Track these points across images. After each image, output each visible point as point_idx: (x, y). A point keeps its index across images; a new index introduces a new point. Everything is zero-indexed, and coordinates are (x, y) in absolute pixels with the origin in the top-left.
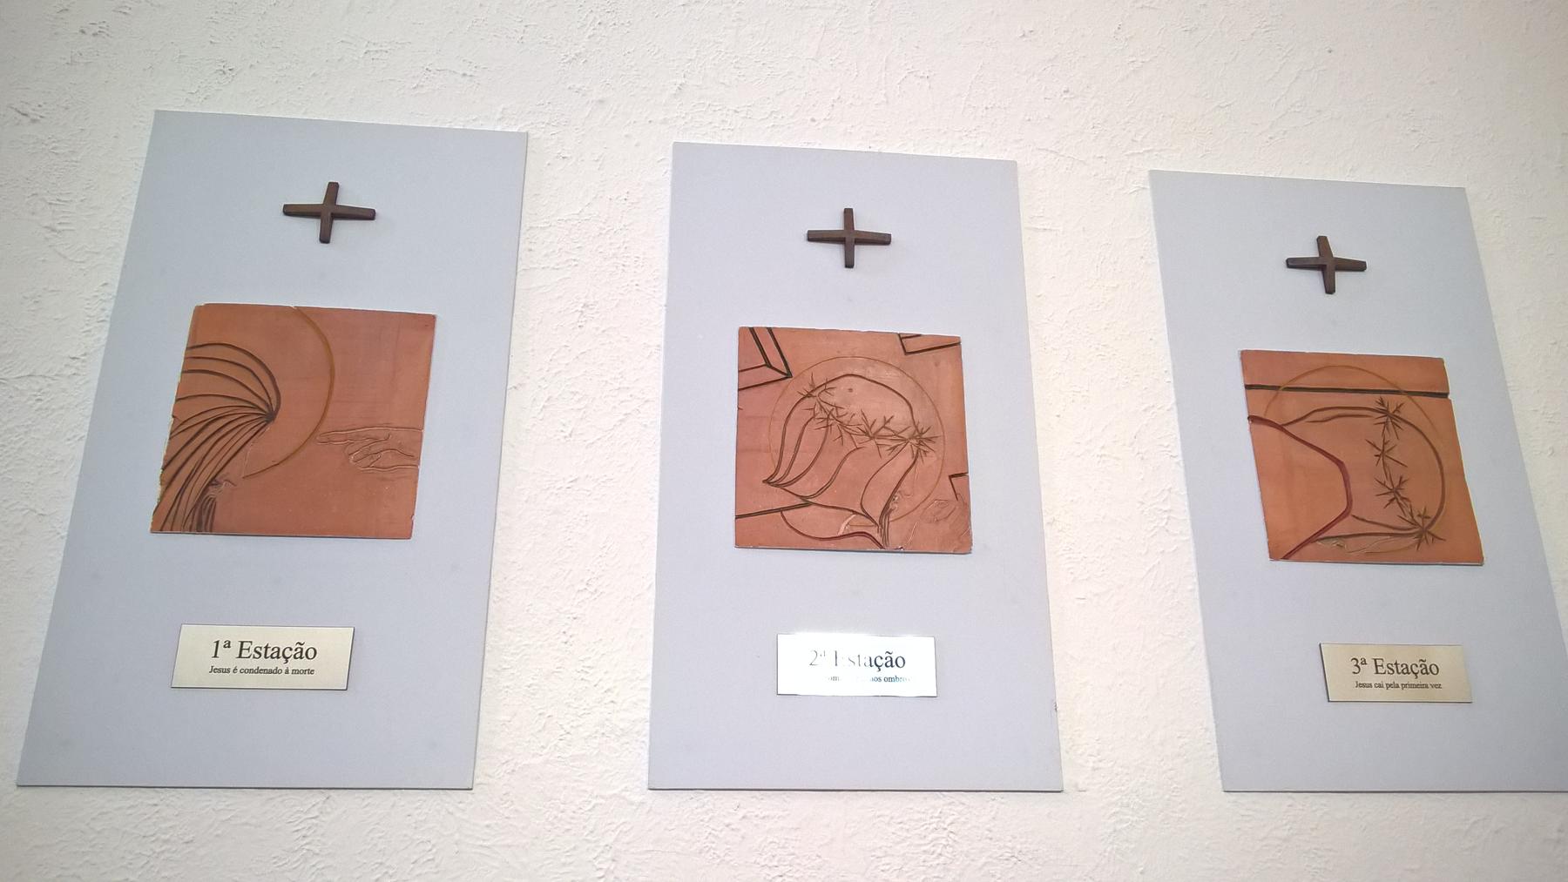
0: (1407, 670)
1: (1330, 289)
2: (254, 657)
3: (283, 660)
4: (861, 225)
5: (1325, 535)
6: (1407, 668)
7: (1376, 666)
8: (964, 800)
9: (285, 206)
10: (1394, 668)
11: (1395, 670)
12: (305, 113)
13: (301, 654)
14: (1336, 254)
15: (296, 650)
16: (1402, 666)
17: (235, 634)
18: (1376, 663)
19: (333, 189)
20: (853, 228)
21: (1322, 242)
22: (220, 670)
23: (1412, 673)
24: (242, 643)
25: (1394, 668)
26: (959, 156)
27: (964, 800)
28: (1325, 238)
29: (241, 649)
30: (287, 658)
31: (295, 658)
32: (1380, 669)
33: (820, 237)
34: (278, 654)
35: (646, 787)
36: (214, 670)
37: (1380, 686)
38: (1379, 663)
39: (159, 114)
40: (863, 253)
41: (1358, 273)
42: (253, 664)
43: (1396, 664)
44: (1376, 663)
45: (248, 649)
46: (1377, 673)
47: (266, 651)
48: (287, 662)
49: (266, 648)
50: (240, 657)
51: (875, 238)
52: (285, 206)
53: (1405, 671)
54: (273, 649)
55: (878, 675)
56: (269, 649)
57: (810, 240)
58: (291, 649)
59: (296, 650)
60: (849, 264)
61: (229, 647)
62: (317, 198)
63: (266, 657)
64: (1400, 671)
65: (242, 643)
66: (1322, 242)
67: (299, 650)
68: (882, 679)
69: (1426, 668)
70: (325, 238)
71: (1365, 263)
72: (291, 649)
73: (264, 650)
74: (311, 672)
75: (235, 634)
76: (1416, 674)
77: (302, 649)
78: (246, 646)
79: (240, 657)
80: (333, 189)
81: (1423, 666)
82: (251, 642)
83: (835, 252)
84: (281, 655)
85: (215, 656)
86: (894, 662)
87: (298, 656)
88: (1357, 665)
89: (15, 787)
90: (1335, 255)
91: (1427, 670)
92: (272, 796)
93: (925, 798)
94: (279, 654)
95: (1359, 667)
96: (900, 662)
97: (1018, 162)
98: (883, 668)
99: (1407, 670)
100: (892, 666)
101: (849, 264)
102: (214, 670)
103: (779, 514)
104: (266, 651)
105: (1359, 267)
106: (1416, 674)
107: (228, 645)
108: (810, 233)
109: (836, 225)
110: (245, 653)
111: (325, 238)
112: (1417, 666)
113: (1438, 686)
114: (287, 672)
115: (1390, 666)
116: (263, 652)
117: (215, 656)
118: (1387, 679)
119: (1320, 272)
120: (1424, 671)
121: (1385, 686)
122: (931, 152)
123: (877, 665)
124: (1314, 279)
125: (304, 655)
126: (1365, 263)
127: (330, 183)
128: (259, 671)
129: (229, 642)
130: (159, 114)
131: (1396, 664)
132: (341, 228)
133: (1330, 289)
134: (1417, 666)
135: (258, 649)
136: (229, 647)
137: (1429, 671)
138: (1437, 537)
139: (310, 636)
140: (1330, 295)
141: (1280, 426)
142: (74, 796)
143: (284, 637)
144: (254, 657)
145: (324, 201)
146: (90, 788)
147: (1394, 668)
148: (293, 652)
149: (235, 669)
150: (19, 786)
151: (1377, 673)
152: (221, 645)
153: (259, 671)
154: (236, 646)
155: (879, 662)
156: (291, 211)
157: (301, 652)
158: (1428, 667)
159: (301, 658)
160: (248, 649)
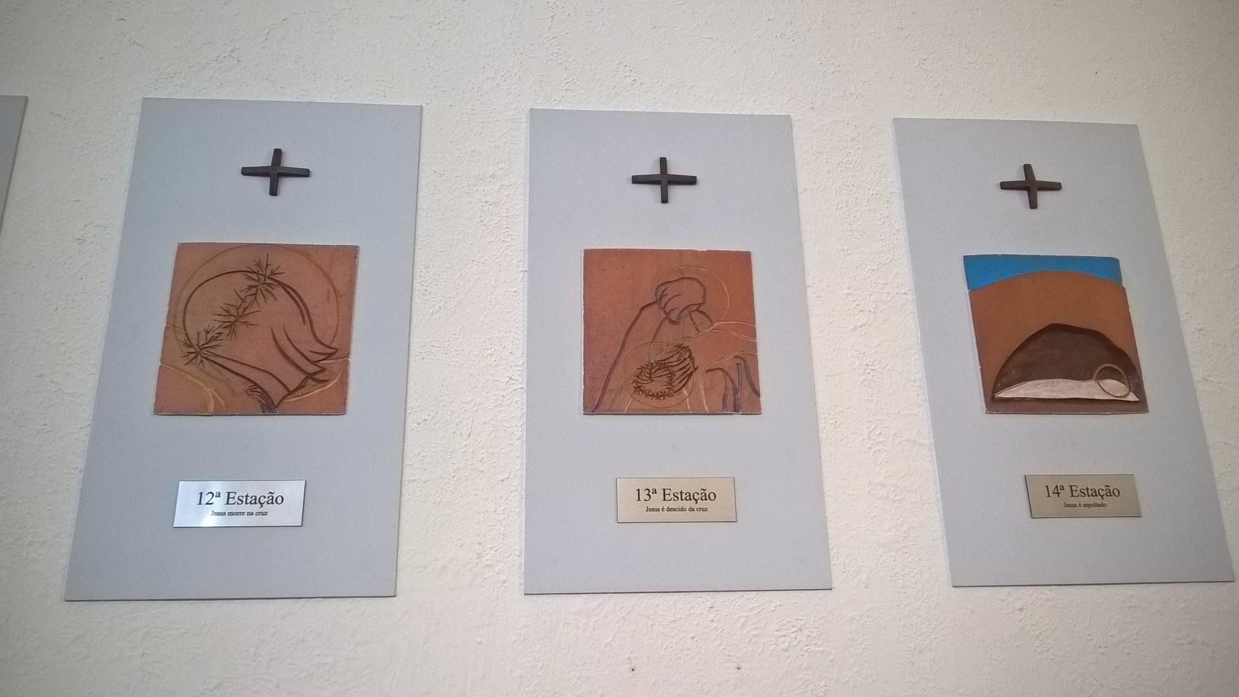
0: (690, 497)
3: (259, 505)
7: (1072, 491)
9: (243, 168)
10: (1086, 493)
11: (680, 497)
12: (598, 108)
15: (268, 497)
16: (1092, 490)
18: (664, 492)
19: (278, 154)
21: (1028, 169)
23: (693, 500)
25: (1086, 493)
26: (1013, 119)
28: (665, 158)
30: (262, 504)
31: (702, 499)
32: (1075, 493)
34: (706, 497)
35: (523, 593)
38: (1074, 488)
40: (676, 192)
42: (673, 504)
43: (1087, 489)
44: (664, 492)
45: (669, 494)
49: (247, 496)
50: (228, 503)
52: (243, 168)
53: (688, 498)
54: (251, 498)
56: (683, 494)
59: (268, 497)
60: (665, 200)
61: (656, 493)
62: (265, 161)
63: (246, 503)
64: (1090, 494)
66: (1028, 169)
67: (271, 498)
68: (254, 513)
70: (274, 192)
71: (1060, 184)
72: (265, 497)
73: (245, 498)
76: (1102, 496)
77: (273, 497)
78: (667, 492)
79: (228, 503)
80: (278, 154)
83: (653, 192)
84: (257, 501)
85: (200, 504)
86: (274, 499)
87: (270, 502)
88: (648, 495)
90: (1037, 179)
91: (706, 497)
95: (650, 496)
96: (712, 496)
97: (792, 116)
98: (699, 501)
99: (690, 497)
100: (706, 499)
101: (665, 200)
103: (291, 390)
104: (246, 499)
107: (655, 492)
110: (231, 501)
111: (274, 192)
114: (663, 509)
116: (244, 499)
117: (639, 500)
118: (673, 504)
119: (1026, 192)
120: (1109, 494)
122: (598, 108)
123: (695, 499)
124: (1019, 198)
125: (707, 498)
126: (1060, 184)
129: (219, 493)
132: (287, 184)
136: (219, 496)
137: (1112, 494)
138: (288, 395)
139: (280, 488)
140: (273, 197)
144: (238, 504)
147: (678, 496)
148: (700, 496)
150: (525, 594)
151: (1072, 496)
152: (1059, 488)
154: (660, 493)
156: (247, 172)
158: (1112, 492)
159: (272, 503)
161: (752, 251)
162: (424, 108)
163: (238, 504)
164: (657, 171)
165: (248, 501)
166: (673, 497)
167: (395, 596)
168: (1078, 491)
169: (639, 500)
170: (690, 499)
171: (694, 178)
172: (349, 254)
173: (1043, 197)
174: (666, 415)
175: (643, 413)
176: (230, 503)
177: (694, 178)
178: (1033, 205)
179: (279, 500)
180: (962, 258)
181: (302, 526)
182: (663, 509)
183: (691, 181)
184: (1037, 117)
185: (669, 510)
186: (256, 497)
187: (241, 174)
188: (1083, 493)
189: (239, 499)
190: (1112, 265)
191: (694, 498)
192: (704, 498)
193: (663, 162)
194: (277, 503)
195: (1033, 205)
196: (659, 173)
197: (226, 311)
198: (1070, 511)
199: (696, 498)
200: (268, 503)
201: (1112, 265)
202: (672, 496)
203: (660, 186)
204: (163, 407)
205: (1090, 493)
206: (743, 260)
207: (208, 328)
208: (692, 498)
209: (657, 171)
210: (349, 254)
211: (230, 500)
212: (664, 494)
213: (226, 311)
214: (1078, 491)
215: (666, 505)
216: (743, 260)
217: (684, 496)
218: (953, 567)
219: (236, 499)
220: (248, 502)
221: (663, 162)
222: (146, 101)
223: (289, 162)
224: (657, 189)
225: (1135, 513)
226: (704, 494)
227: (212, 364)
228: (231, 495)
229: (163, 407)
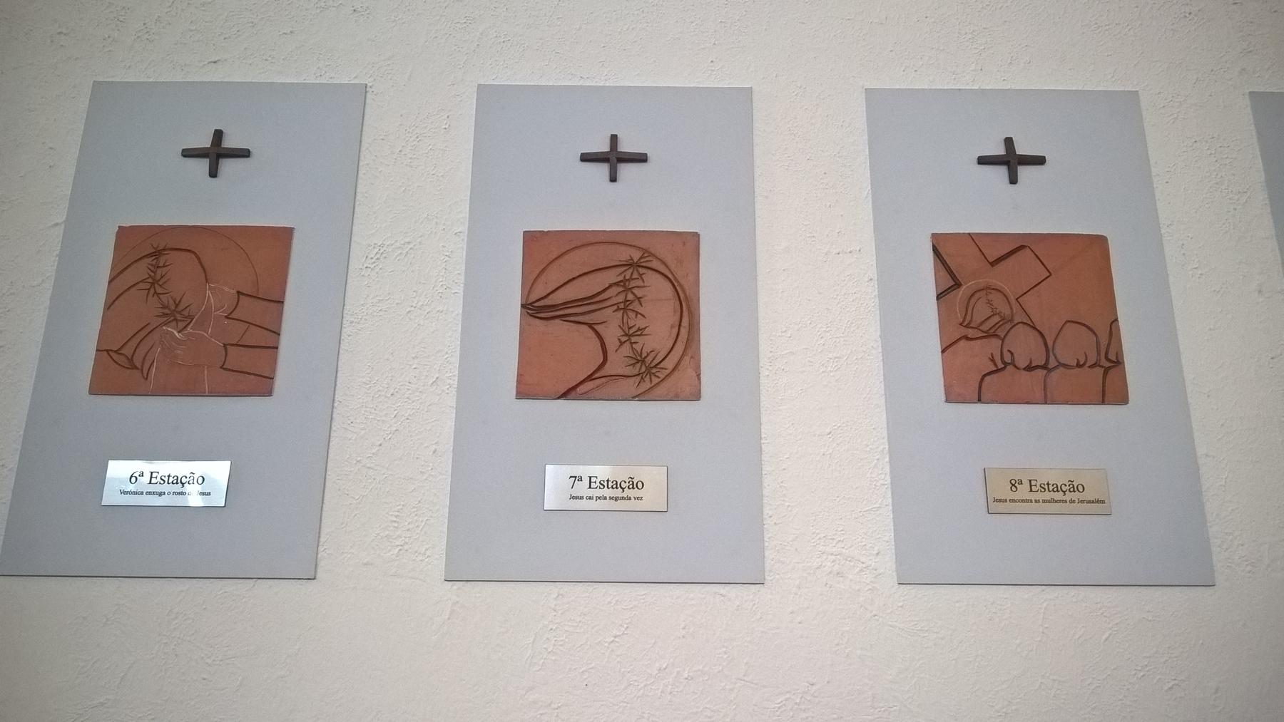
0: (1057, 489)
2: (600, 488)
4: (1021, 150)
5: (596, 376)
8: (722, 591)
9: (183, 150)
10: (166, 479)
15: (1069, 485)
17: (585, 471)
18: (1030, 484)
19: (218, 135)
21: (1009, 142)
23: (1061, 492)
24: (152, 473)
25: (1046, 487)
27: (722, 591)
28: (1011, 138)
29: (151, 477)
30: (183, 484)
33: (197, 152)
36: (572, 497)
37: (591, 498)
39: (96, 85)
40: (625, 170)
45: (156, 478)
46: (1031, 491)
48: (624, 491)
49: (169, 476)
50: (150, 483)
51: (632, 157)
53: (1055, 489)
54: (1053, 485)
55: (1064, 498)
59: (1069, 485)
60: (613, 179)
61: (581, 480)
62: (205, 142)
64: (1051, 489)
65: (152, 473)
66: (1009, 142)
67: (1071, 486)
69: (1073, 487)
70: (213, 173)
73: (167, 478)
75: (585, 471)
76: (1064, 492)
77: (633, 482)
78: (1033, 483)
80: (218, 135)
81: (1071, 486)
82: (596, 477)
84: (179, 481)
89: (897, 586)
92: (595, 587)
96: (640, 485)
98: (626, 489)
101: (613, 179)
102: (572, 497)
105: (1039, 161)
106: (1064, 492)
109: (604, 147)
110: (154, 481)
111: (213, 173)
113: (641, 499)
115: (1042, 485)
120: (614, 486)
121: (595, 498)
123: (1063, 491)
125: (635, 486)
128: (1053, 501)
129: (1021, 481)
130: (96, 85)
132: (227, 166)
135: (163, 478)
137: (1076, 489)
139: (641, 474)
140: (1013, 185)
142: (110, 585)
144: (600, 488)
145: (1019, 155)
146: (50, 578)
147: (1044, 488)
148: (627, 484)
151: (1031, 491)
153: (1053, 501)
154: (586, 481)
155: (184, 480)
156: (586, 158)
160: (156, 478)
165: (170, 481)
167: (314, 579)
168: (1038, 486)
174: (207, 396)
175: (224, 394)
178: (1013, 180)
180: (930, 236)
181: (225, 506)
182: (606, 498)
183: (641, 159)
185: (1045, 501)
186: (617, 482)
188: (1044, 488)
190: (1098, 244)
191: (181, 482)
192: (1072, 490)
193: (614, 139)
194: (638, 488)
195: (1013, 180)
199: (183, 481)
200: (173, 483)
201: (1098, 244)
202: (598, 484)
204: (94, 390)
205: (1051, 488)
206: (532, 240)
207: (627, 315)
208: (618, 486)
210: (284, 236)
211: (592, 484)
212: (1031, 486)
214: (1038, 486)
215: (1033, 496)
216: (532, 240)
217: (171, 479)
218: (900, 561)
221: (614, 139)
223: (229, 143)
226: (631, 483)
228: (154, 475)
229: (94, 390)
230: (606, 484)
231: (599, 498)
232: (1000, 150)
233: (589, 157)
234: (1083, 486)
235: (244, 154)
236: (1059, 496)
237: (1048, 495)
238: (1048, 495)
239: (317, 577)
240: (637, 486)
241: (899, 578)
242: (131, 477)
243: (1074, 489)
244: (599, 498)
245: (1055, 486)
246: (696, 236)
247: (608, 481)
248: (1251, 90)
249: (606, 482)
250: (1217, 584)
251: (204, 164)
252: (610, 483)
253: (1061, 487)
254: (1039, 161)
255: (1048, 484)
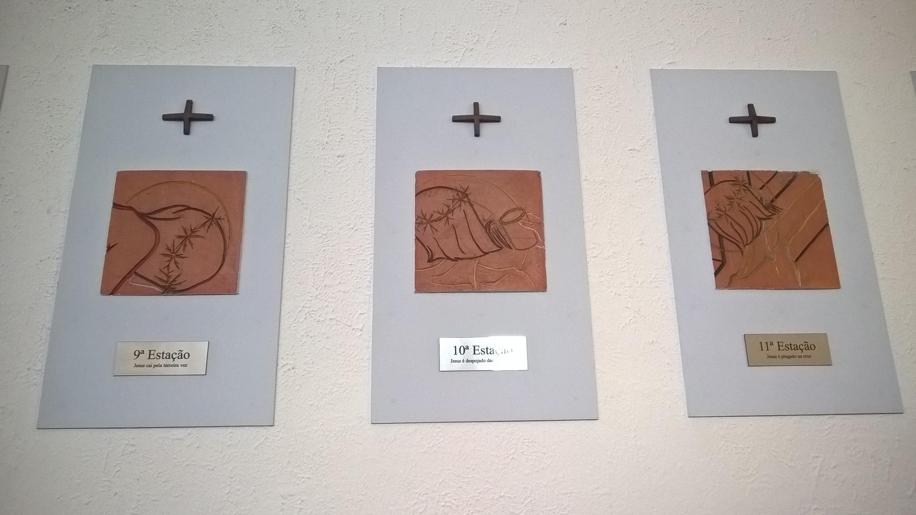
0: (797, 348)
1: (755, 134)
3: (172, 359)
6: (797, 347)
7: (779, 346)
11: (790, 347)
13: (182, 356)
14: (758, 114)
15: (179, 354)
19: (189, 104)
20: (191, 112)
21: (751, 107)
22: (139, 366)
24: (150, 351)
29: (150, 354)
30: (174, 359)
31: (178, 358)
32: (477, 352)
35: (687, 416)
36: (136, 366)
38: (780, 344)
40: (485, 128)
41: (210, 122)
45: (154, 354)
47: (163, 355)
48: (174, 360)
49: (163, 353)
50: (149, 358)
56: (164, 354)
57: (730, 122)
58: (176, 354)
60: (477, 134)
61: (468, 349)
62: (180, 109)
65: (150, 351)
66: (751, 107)
67: (806, 346)
68: (180, 366)
69: (808, 346)
70: (187, 132)
71: (775, 118)
72: (176, 354)
73: (162, 354)
74: (810, 357)
76: (802, 350)
77: (182, 354)
78: (476, 348)
79: (149, 358)
80: (189, 104)
84: (171, 357)
87: (180, 357)
90: (757, 115)
91: (808, 348)
93: (91, 433)
94: (169, 356)
96: (187, 356)
99: (797, 348)
101: (477, 134)
102: (136, 366)
104: (163, 355)
105: (772, 120)
106: (802, 350)
108: (164, 116)
110: (152, 357)
111: (187, 132)
112: (803, 345)
116: (161, 356)
117: (762, 350)
119: (750, 125)
120: (796, 348)
121: (153, 366)
123: (173, 358)
124: (746, 129)
127: (753, 105)
129: (468, 347)
131: (790, 345)
132: (196, 126)
133: (755, 134)
134: (803, 345)
135: (159, 354)
137: (809, 348)
139: (185, 347)
140: (187, 136)
141: (138, 213)
143: (174, 348)
144: (157, 359)
146: (554, 422)
147: (789, 347)
148: (178, 355)
149: (463, 360)
150: (38, 429)
151: (779, 350)
152: (769, 344)
154: (776, 344)
155: (174, 356)
156: (456, 119)
157: (182, 355)
158: (798, 347)
159: (181, 358)
160: (154, 354)
161: (248, 171)
162: (297, 69)
163: (157, 359)
164: (472, 113)
166: (156, 356)
168: (480, 350)
169: (762, 350)
170: (797, 349)
171: (499, 118)
172: (240, 178)
173: (762, 128)
176: (151, 358)
177: (499, 118)
179: (187, 356)
184: (754, 66)
186: (170, 354)
187: (162, 120)
189: (157, 355)
191: (800, 348)
192: (807, 348)
193: (476, 105)
196: (473, 114)
197: (423, 215)
198: (772, 360)
200: (166, 358)
202: (480, 351)
203: (473, 124)
209: (472, 113)
210: (240, 178)
211: (780, 347)
213: (423, 215)
214: (480, 350)
216: (419, 175)
219: (155, 355)
220: (164, 357)
221: (476, 105)
222: (95, 68)
224: (470, 127)
225: (827, 362)
226: (180, 354)
227: (475, 255)
228: (152, 352)
230: (485, 351)
231: (156, 366)
232: (745, 113)
233: (464, 119)
234: (814, 346)
235: (209, 118)
236: (798, 352)
237: (790, 353)
238: (790, 353)
239: (276, 424)
240: (184, 356)
241: (688, 414)
242: (138, 355)
243: (808, 348)
244: (156, 366)
245: (795, 346)
246: (538, 174)
247: (487, 349)
248: (910, 71)
249: (486, 350)
250: (601, 417)
251: (180, 126)
252: (489, 350)
253: (184, 355)
254: (772, 120)
255: (790, 345)
